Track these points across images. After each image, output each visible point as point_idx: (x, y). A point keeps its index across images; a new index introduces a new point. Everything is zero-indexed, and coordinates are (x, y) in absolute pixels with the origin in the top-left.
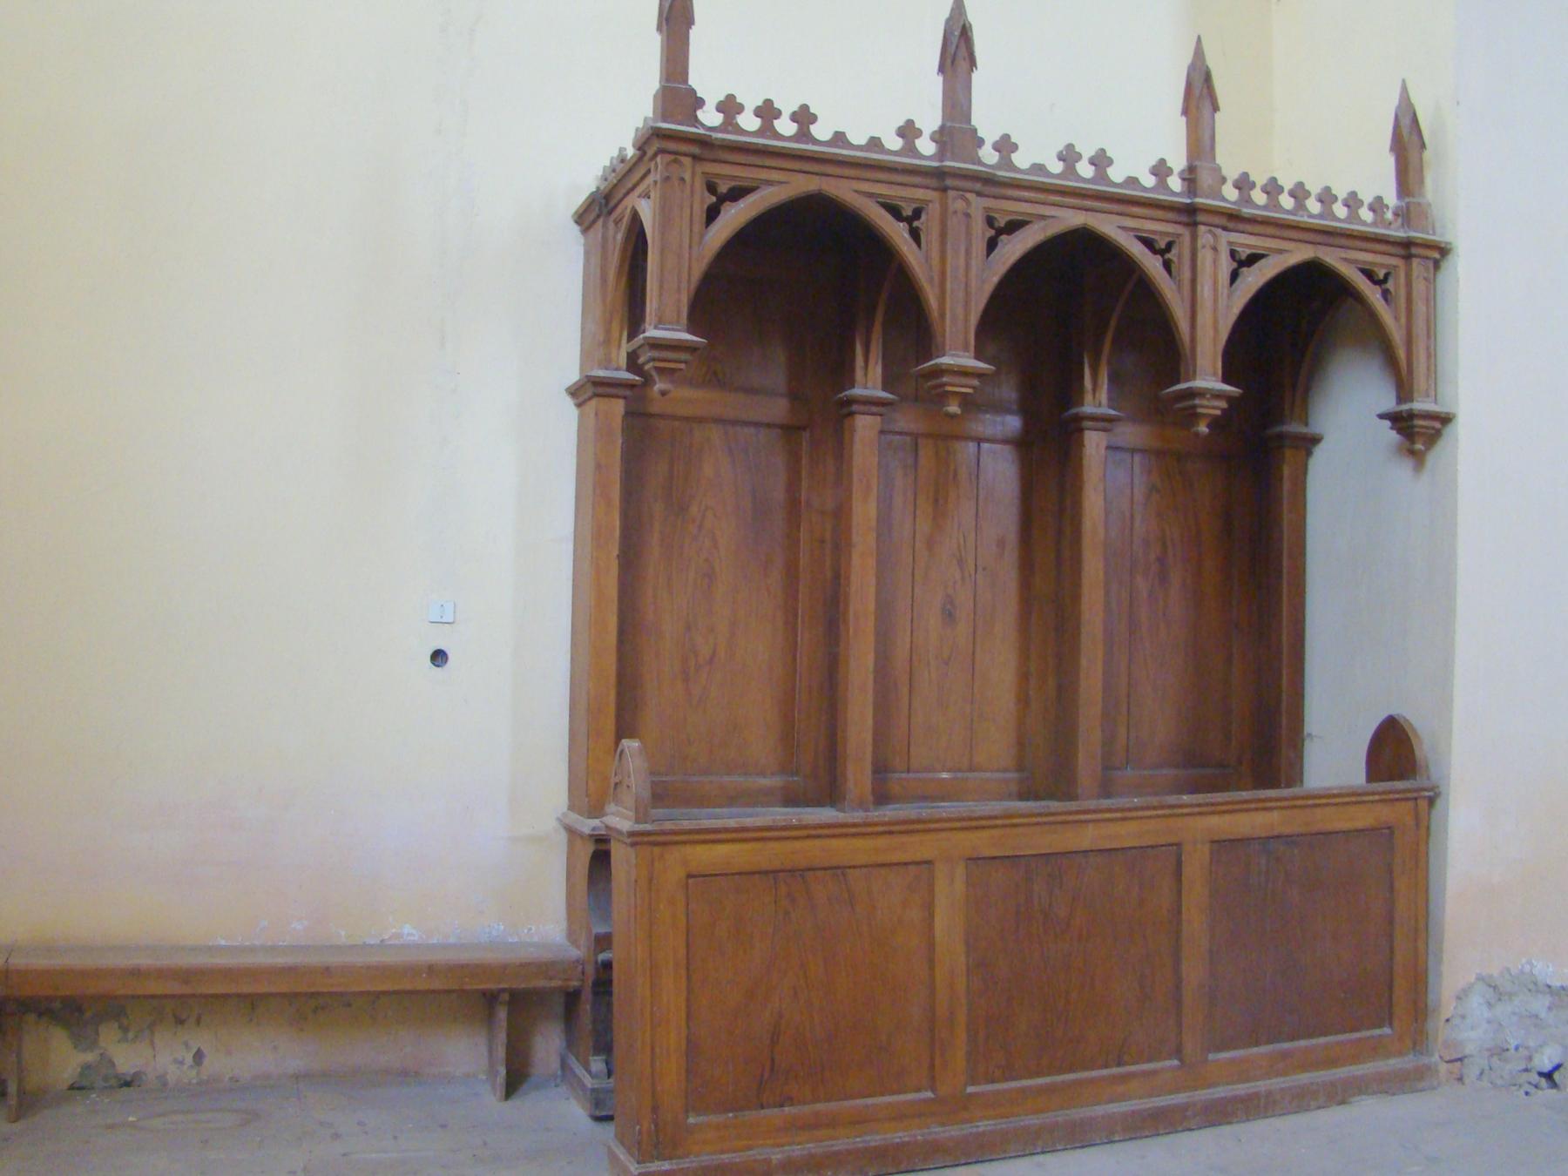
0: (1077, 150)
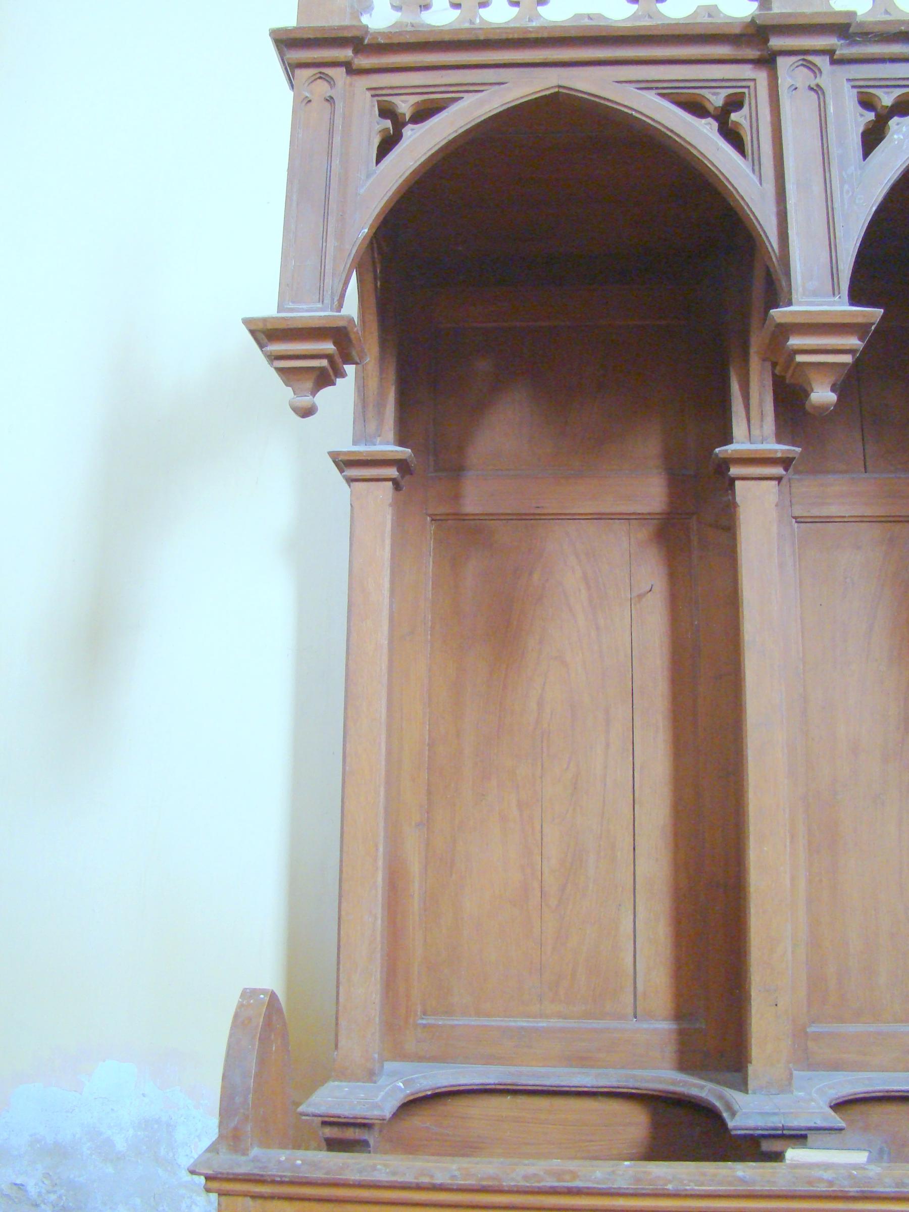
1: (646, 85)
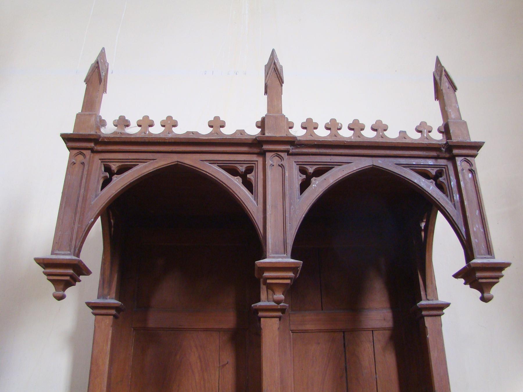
1: (213, 162)
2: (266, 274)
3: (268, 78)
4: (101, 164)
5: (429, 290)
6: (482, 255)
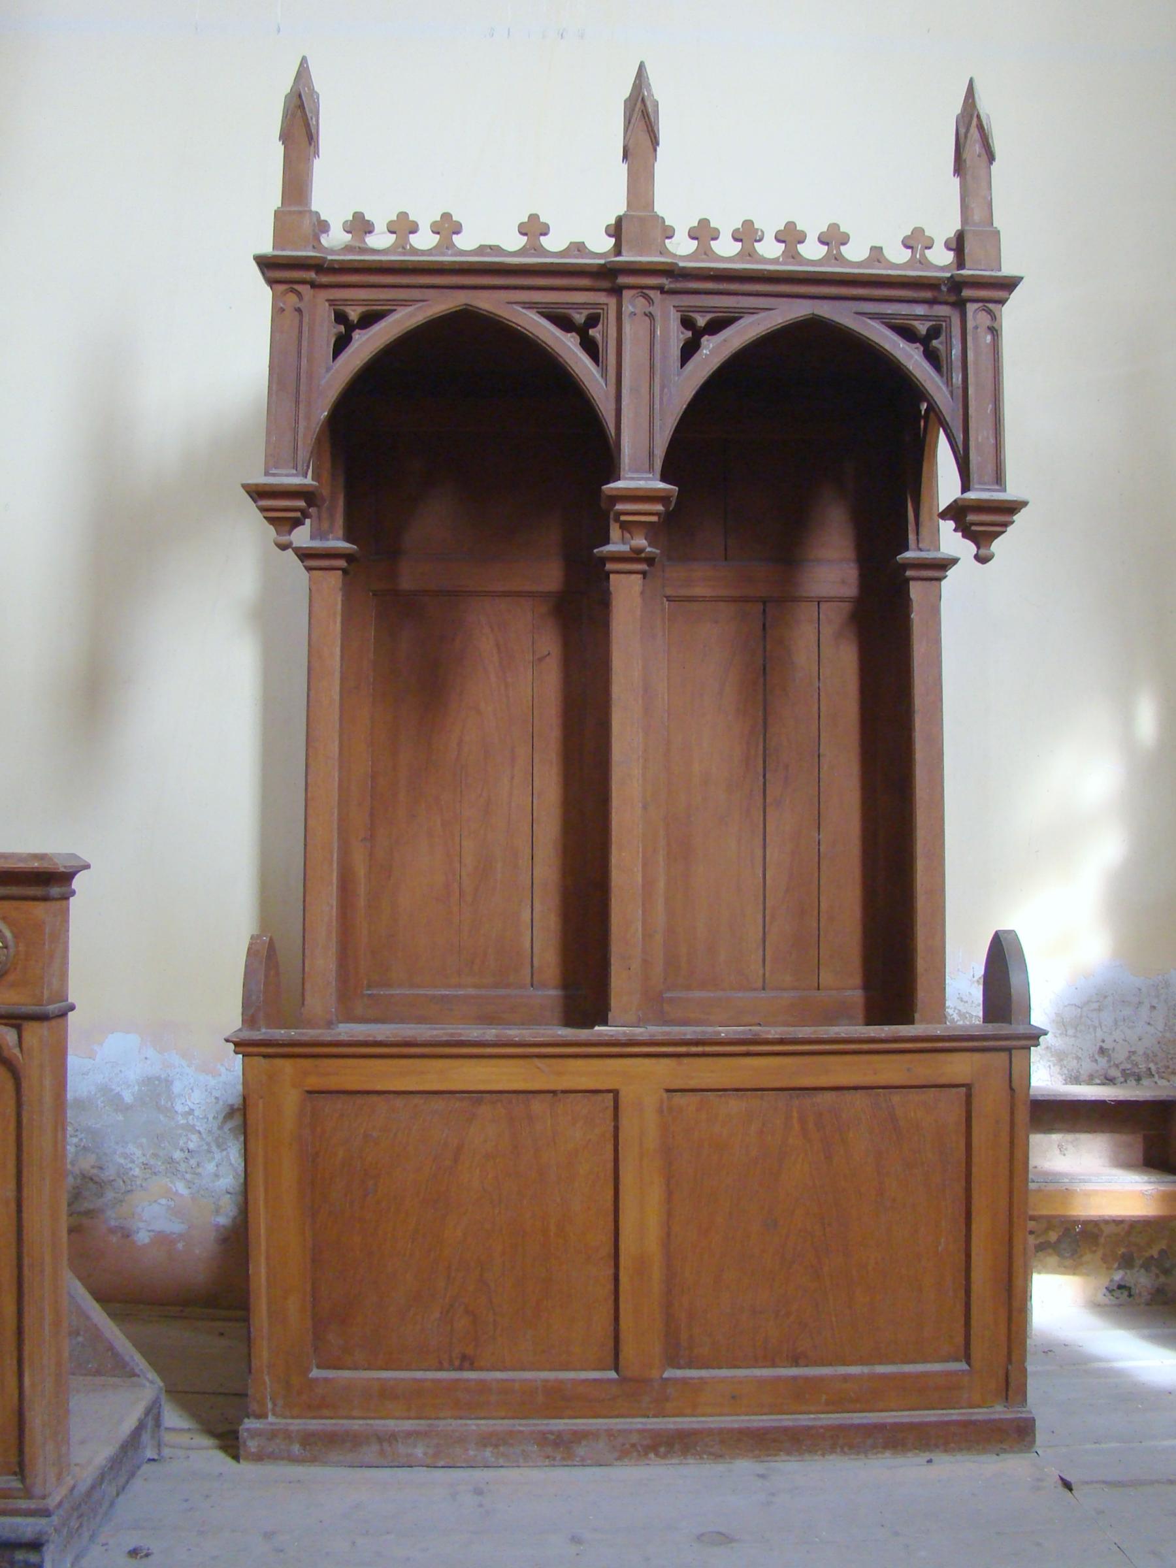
0: (696, 225)
1: (529, 305)
2: (619, 507)
3: (629, 133)
4: (329, 309)
5: (924, 531)
6: (985, 484)
